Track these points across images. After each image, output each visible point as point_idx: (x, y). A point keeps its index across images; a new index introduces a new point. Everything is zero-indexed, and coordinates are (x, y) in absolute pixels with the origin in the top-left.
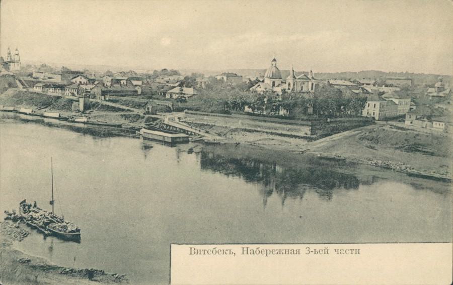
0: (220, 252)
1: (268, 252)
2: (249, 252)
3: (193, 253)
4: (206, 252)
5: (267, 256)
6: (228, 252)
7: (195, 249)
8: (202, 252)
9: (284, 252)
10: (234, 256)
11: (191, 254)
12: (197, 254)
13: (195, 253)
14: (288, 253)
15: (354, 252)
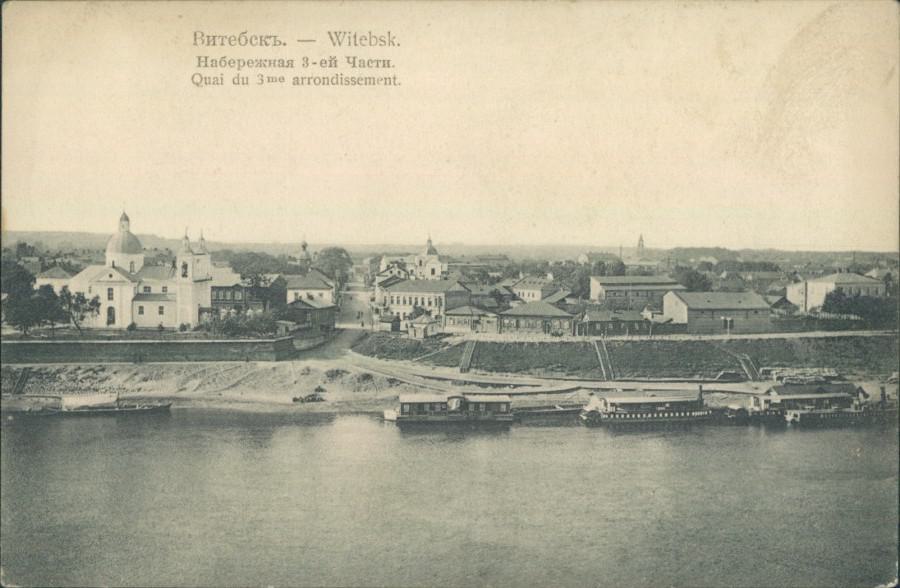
0: (254, 42)
2: (209, 63)
4: (226, 41)
12: (208, 44)
14: (274, 66)
15: (381, 64)
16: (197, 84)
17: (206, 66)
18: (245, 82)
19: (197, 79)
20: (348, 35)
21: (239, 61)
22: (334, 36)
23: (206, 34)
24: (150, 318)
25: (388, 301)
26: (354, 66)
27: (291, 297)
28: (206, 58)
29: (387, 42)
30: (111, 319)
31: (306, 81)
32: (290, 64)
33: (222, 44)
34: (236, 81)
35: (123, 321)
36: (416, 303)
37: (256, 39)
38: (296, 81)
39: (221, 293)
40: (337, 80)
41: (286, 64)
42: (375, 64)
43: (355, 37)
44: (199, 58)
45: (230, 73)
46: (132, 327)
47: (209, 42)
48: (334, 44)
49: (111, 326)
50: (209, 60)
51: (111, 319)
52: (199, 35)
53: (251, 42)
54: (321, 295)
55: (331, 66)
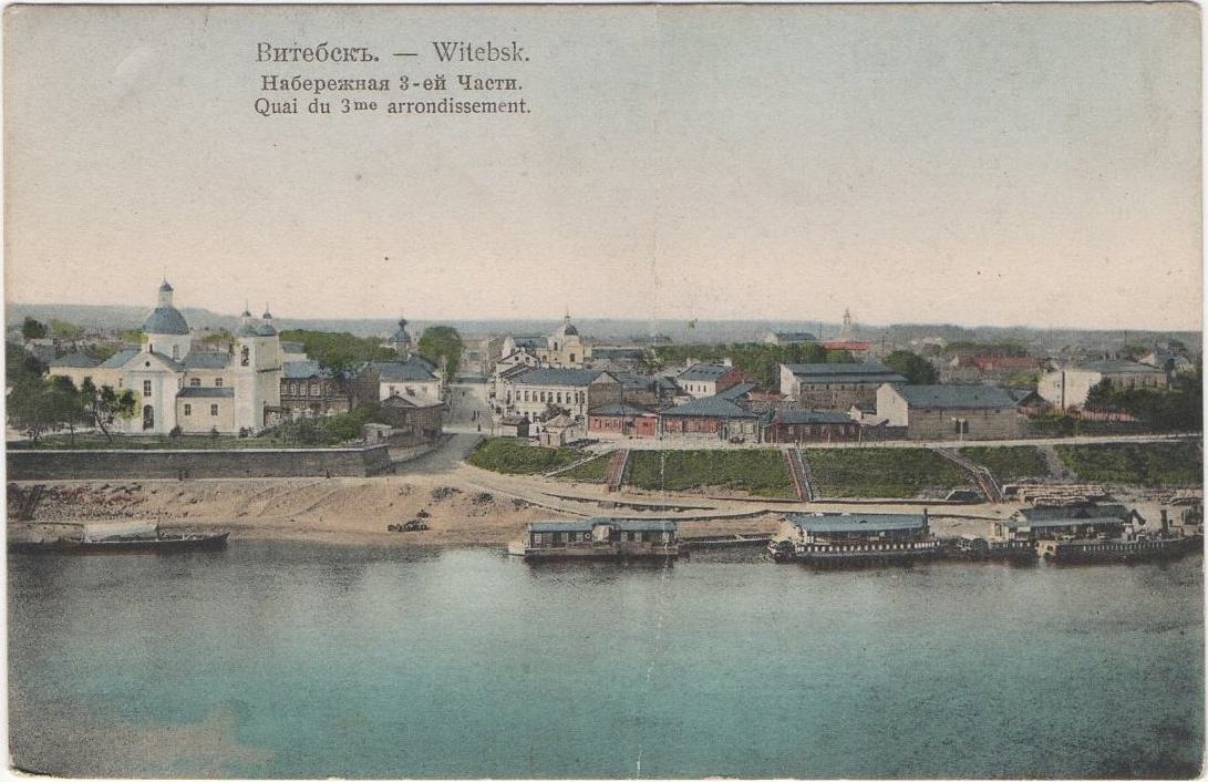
0: (337, 56)
2: (278, 85)
3: (265, 56)
4: (300, 55)
8: (290, 56)
9: (354, 85)
10: (344, 112)
15: (504, 85)
16: (262, 112)
18: (326, 109)
19: (262, 106)
20: (459, 46)
21: (317, 82)
22: (440, 46)
23: (273, 46)
24: (200, 420)
25: (513, 397)
26: (468, 88)
27: (385, 392)
28: (468, 77)
29: (512, 57)
30: (148, 423)
31: (405, 108)
32: (385, 85)
33: (296, 59)
34: (313, 109)
35: (165, 425)
36: (550, 399)
37: (339, 52)
38: (392, 109)
39: (293, 387)
40: (446, 107)
41: (378, 85)
42: (496, 85)
43: (469, 49)
44: (443, 88)
45: (305, 98)
46: (176, 431)
48: (442, 59)
49: (150, 431)
50: (278, 80)
51: (148, 423)
52: (264, 48)
53: (332, 56)
54: (425, 389)
55: (437, 88)
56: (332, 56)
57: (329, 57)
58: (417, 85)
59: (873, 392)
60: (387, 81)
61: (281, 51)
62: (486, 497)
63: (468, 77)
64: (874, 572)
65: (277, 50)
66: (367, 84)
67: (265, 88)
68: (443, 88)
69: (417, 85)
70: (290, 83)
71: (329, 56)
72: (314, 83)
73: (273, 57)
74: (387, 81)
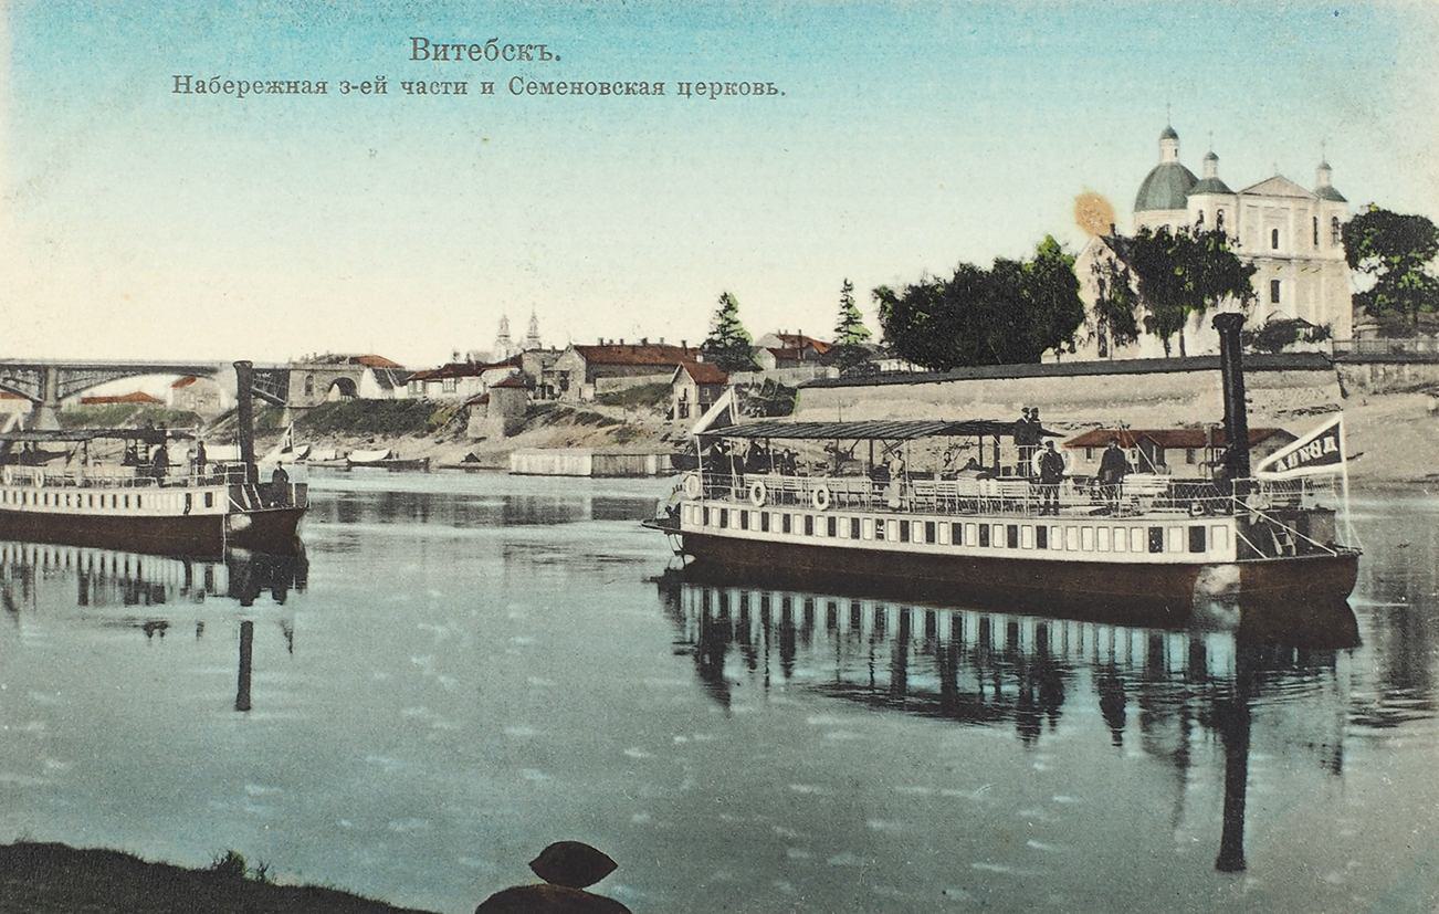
0: (509, 54)
1: (244, 87)
2: (193, 85)
3: (421, 54)
4: (464, 54)
5: (712, 98)
6: (535, 53)
7: (427, 42)
8: (452, 54)
9: (284, 88)
11: (415, 58)
12: (377, 91)
13: (428, 55)
15: (451, 90)
17: (188, 91)
23: (432, 42)
28: (188, 78)
42: (442, 89)
44: (464, 92)
47: (436, 55)
52: (421, 44)
56: (225, 88)
57: (251, 90)
58: (357, 87)
59: (1252, 430)
60: (662, 84)
61: (441, 48)
62: (456, 540)
63: (188, 78)
64: (1187, 660)
65: (436, 46)
66: (300, 87)
67: (415, 58)
68: (464, 92)
69: (357, 87)
70: (724, 91)
71: (222, 86)
72: (237, 85)
73: (432, 56)
74: (662, 84)
